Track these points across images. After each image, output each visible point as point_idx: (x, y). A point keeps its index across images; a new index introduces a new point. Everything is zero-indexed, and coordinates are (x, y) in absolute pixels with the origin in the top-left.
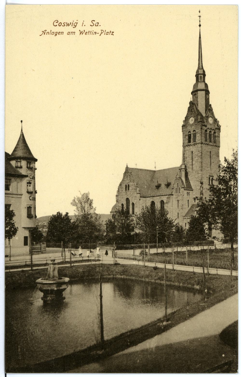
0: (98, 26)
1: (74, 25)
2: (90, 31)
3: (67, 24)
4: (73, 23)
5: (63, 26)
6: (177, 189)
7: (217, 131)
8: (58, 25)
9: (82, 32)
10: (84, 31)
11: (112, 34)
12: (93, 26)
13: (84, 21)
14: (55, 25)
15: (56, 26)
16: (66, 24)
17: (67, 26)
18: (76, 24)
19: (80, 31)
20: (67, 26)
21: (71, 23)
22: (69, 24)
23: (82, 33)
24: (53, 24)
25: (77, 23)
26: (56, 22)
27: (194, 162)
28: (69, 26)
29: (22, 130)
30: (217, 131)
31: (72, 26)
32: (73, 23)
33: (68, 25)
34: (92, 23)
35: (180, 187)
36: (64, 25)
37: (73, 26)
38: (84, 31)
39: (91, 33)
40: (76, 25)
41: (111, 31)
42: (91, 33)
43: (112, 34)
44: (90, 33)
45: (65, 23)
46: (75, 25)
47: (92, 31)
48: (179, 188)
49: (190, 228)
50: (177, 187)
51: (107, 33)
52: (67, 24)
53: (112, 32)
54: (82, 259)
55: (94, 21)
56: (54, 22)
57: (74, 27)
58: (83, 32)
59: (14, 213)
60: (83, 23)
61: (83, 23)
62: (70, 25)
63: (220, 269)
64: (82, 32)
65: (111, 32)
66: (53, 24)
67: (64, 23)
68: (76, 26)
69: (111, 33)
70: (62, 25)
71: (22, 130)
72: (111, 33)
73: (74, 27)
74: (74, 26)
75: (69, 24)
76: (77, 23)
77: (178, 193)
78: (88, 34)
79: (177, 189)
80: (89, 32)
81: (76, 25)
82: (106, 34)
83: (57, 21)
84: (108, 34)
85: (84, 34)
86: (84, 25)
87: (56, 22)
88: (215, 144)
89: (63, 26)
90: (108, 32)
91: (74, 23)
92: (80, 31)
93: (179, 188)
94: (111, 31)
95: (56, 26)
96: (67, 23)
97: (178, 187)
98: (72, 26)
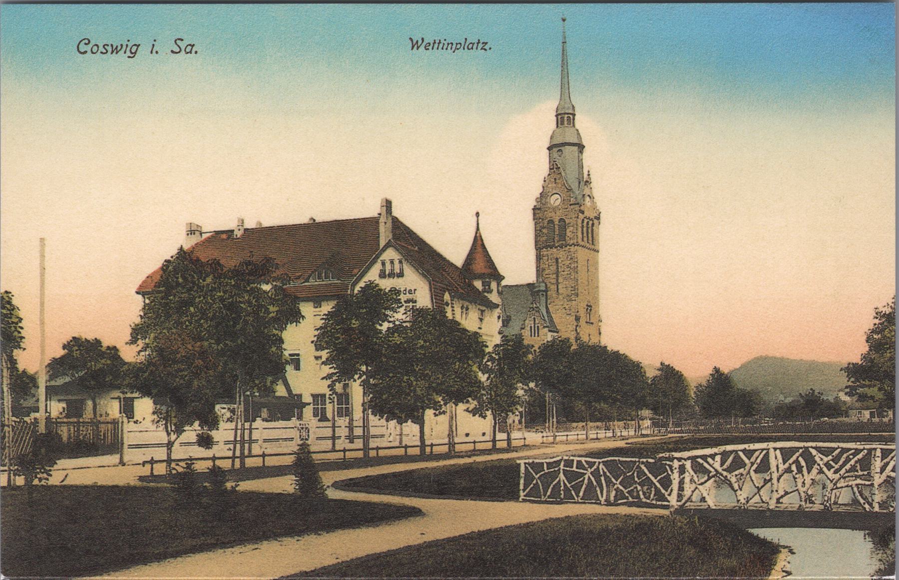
0: (191, 52)
1: (131, 51)
2: (437, 41)
3: (112, 48)
4: (127, 45)
5: (102, 53)
6: (533, 328)
7: (596, 221)
8: (89, 52)
9: (417, 42)
10: (423, 39)
11: (482, 49)
12: (179, 52)
13: (128, 41)
14: (82, 51)
15: (85, 52)
16: (109, 49)
17: (112, 53)
18: (135, 48)
19: (411, 39)
20: (112, 53)
21: (122, 45)
22: (119, 48)
23: (416, 45)
24: (78, 47)
25: (139, 45)
26: (86, 44)
27: (560, 280)
28: (117, 53)
29: (478, 229)
30: (596, 221)
31: (125, 52)
32: (127, 45)
33: (115, 50)
34: (176, 46)
35: (539, 325)
36: (105, 51)
37: (128, 53)
38: (423, 39)
39: (436, 46)
40: (136, 51)
41: (479, 40)
42: (441, 45)
43: (482, 49)
44: (436, 46)
45: (108, 45)
46: (133, 51)
47: (442, 41)
48: (536, 328)
49: (214, 408)
50: (533, 326)
51: (470, 46)
52: (112, 48)
53: (483, 43)
54: (473, 448)
55: (172, 52)
56: (79, 44)
57: (129, 57)
58: (419, 44)
59: (672, 367)
60: (153, 45)
61: (153, 45)
62: (120, 50)
63: (287, 464)
64: (417, 42)
65: (481, 41)
66: (78, 47)
67: (179, 39)
68: (135, 53)
69: (480, 46)
70: (99, 51)
71: (478, 229)
72: (480, 46)
73: (129, 57)
74: (132, 53)
75: (119, 48)
76: (139, 45)
77: (535, 336)
78: (433, 49)
79: (533, 328)
80: (435, 42)
81: (136, 51)
82: (468, 49)
83: (87, 41)
84: (472, 48)
85: (422, 48)
86: (154, 51)
87: (86, 44)
88: (593, 247)
89: (102, 53)
90: (473, 44)
91: (130, 44)
92: (411, 39)
93: (538, 327)
94: (479, 40)
95: (85, 52)
96: (112, 46)
97: (536, 326)
98: (125, 52)
